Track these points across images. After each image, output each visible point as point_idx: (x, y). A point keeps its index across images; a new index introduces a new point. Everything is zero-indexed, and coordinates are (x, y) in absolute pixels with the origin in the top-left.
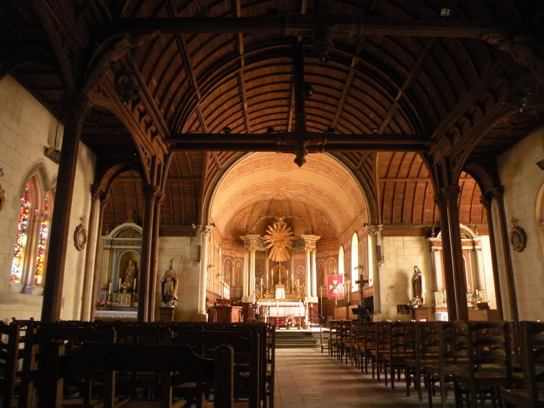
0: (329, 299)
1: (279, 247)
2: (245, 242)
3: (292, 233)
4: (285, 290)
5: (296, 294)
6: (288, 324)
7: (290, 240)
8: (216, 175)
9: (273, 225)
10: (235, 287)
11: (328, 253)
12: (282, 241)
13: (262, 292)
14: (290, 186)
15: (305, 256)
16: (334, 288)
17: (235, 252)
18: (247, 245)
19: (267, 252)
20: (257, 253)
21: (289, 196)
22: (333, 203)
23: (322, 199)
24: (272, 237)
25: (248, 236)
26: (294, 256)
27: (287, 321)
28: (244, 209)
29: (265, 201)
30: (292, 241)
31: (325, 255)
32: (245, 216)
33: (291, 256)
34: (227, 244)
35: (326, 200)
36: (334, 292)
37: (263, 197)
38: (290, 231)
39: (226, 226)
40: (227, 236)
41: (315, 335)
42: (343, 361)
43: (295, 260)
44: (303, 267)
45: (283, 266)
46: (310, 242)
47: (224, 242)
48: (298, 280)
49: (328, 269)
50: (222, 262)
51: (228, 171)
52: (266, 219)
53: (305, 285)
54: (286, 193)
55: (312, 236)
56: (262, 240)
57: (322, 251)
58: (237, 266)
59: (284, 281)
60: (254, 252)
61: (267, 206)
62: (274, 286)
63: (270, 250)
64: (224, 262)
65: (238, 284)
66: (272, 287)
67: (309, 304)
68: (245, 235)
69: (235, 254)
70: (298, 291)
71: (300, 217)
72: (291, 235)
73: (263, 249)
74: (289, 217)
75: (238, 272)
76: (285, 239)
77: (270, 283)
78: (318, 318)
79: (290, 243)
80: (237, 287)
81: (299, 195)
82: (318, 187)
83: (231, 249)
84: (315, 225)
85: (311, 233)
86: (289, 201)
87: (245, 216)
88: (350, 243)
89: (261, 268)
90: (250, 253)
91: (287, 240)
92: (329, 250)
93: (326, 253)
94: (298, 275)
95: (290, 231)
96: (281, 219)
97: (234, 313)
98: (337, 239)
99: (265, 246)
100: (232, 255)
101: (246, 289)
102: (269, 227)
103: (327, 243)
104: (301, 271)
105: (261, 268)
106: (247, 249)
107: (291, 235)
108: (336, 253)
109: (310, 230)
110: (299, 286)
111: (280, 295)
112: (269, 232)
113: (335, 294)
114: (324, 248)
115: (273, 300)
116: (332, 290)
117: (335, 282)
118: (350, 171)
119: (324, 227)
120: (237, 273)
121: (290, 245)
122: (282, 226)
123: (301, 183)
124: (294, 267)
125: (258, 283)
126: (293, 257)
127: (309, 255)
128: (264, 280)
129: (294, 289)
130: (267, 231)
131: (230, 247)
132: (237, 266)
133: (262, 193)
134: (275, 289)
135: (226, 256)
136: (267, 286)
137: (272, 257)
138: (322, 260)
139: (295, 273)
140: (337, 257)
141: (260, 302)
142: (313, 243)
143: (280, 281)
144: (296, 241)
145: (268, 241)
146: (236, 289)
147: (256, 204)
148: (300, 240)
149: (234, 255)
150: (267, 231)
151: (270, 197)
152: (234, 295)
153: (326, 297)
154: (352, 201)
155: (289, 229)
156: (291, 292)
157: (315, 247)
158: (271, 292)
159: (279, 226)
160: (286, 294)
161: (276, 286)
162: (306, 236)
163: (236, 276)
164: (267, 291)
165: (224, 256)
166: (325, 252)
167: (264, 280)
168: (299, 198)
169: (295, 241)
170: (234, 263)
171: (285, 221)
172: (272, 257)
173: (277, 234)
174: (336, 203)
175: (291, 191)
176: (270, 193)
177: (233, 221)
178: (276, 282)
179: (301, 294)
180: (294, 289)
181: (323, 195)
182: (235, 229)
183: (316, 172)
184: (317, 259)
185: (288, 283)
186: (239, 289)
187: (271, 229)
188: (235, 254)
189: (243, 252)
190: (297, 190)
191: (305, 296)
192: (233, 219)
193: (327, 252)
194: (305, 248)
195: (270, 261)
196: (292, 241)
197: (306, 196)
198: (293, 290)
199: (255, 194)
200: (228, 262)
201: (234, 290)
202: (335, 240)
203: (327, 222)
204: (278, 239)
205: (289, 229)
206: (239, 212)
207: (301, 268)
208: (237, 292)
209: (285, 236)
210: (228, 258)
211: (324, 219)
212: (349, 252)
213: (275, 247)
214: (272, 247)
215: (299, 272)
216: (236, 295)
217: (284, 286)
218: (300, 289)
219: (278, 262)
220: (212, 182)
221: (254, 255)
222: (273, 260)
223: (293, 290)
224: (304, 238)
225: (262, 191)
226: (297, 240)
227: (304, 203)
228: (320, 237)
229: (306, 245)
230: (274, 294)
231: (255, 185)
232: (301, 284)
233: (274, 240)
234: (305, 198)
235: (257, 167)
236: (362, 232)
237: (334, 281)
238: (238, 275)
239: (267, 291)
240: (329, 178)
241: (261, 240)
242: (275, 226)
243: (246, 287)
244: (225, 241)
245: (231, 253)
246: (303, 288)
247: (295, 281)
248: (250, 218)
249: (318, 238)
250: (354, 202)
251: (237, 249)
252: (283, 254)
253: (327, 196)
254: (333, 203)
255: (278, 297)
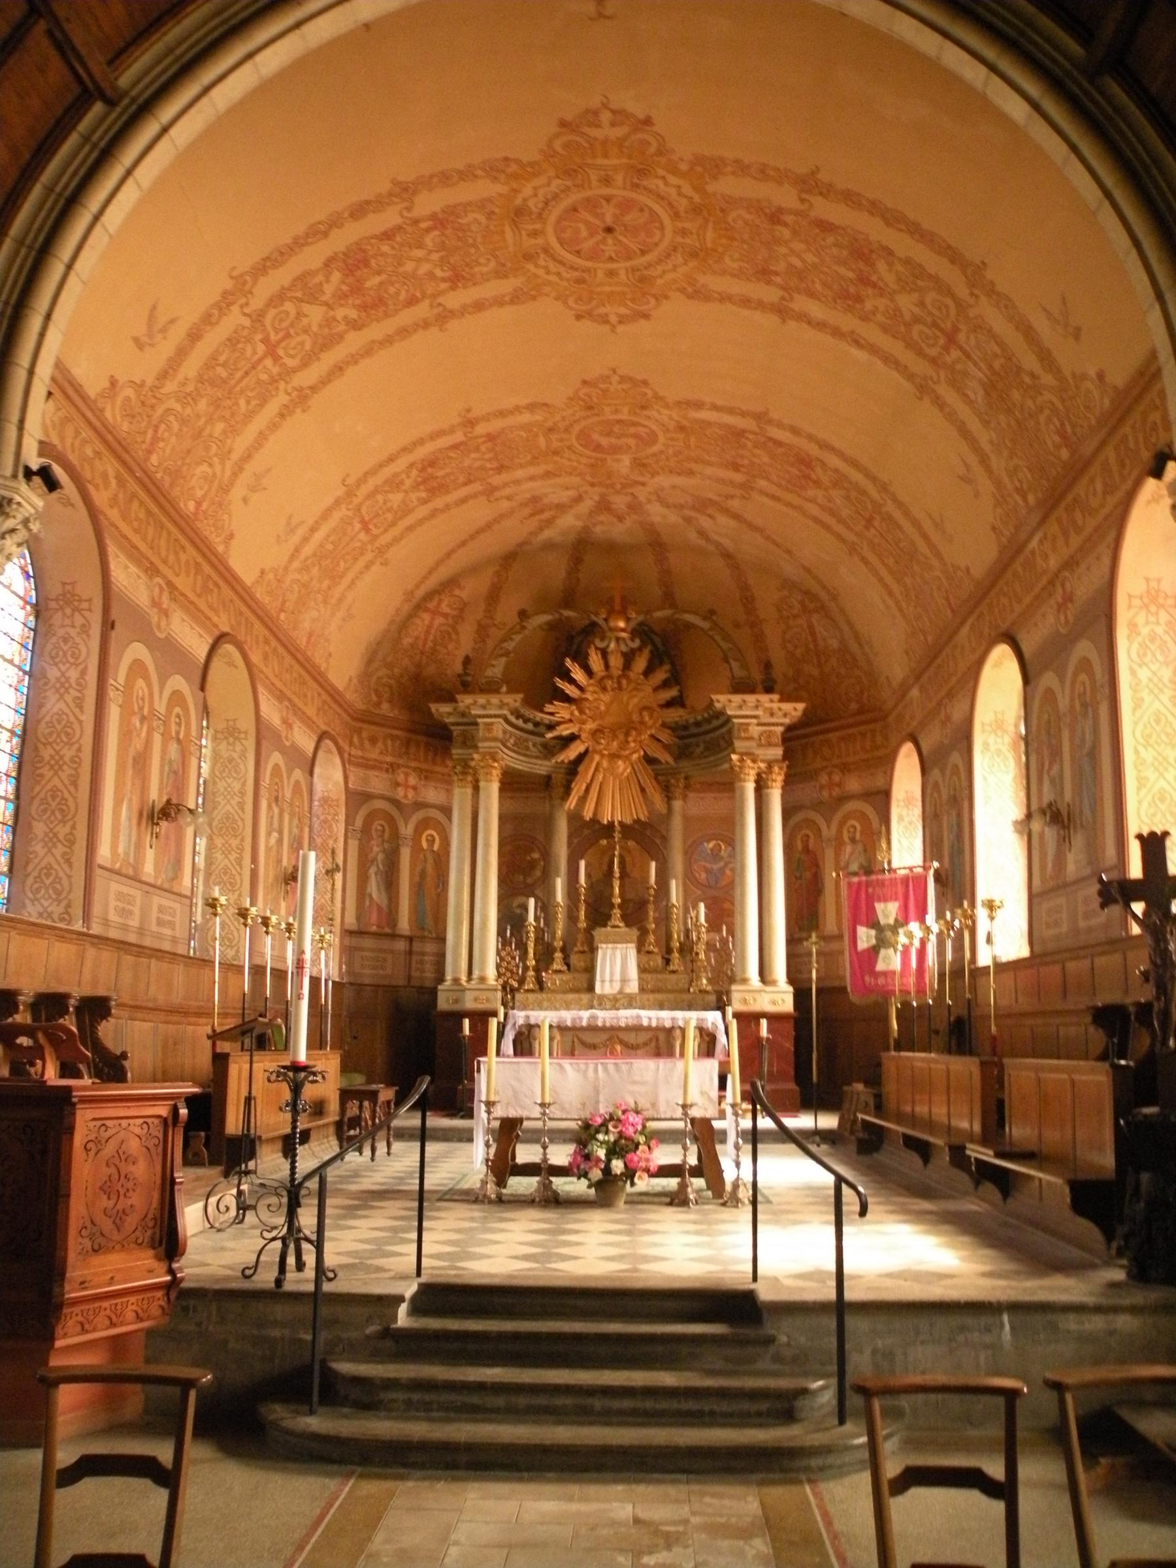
0: (854, 998)
1: (614, 757)
2: (456, 731)
3: (673, 693)
4: (639, 951)
5: (693, 972)
6: (607, 1171)
7: (664, 725)
8: (73, 140)
9: (587, 655)
10: (410, 939)
11: (839, 785)
12: (627, 727)
13: (531, 962)
14: (653, 438)
15: (732, 798)
16: (883, 942)
17: (412, 780)
18: (464, 744)
19: (558, 778)
20: (512, 783)
21: (657, 513)
22: (869, 522)
23: (813, 509)
24: (581, 712)
25: (465, 700)
26: (685, 798)
27: (601, 1153)
28: (451, 583)
29: (549, 546)
30: (674, 728)
31: (825, 794)
32: (460, 617)
33: (669, 799)
34: (373, 740)
35: (832, 513)
36: (880, 966)
37: (534, 523)
38: (665, 684)
39: (370, 661)
40: (378, 704)
41: (784, 1332)
42: (556, 444)
43: (687, 819)
44: (724, 851)
45: (631, 843)
46: (755, 730)
47: (359, 731)
48: (702, 906)
49: (837, 855)
50: (349, 821)
51: (167, 112)
52: (552, 627)
53: (731, 932)
54: (642, 494)
55: (764, 698)
56: (536, 724)
57: (810, 776)
58: (425, 845)
59: (634, 915)
60: (496, 774)
61: (563, 574)
62: (589, 931)
63: (573, 769)
64: (359, 822)
65: (429, 922)
66: (581, 937)
67: (756, 1017)
68: (452, 699)
69: (415, 788)
70: (702, 956)
71: (710, 614)
72: (669, 704)
73: (542, 767)
74: (659, 614)
75: (430, 869)
76: (642, 723)
77: (572, 918)
78: (792, 1086)
79: (665, 737)
80: (423, 939)
81: (703, 505)
82: (795, 431)
83: (393, 768)
84: (777, 655)
85: (760, 687)
86: (656, 544)
87: (460, 617)
88: (957, 714)
89: (536, 855)
90: (476, 789)
91: (652, 725)
92: (845, 768)
93: (831, 785)
94: (697, 883)
95: (665, 684)
96: (622, 624)
97: (95, 1145)
98: (885, 718)
99: (549, 750)
100: (400, 792)
101: (457, 945)
102: (568, 662)
103: (832, 736)
104: (715, 867)
105: (536, 855)
106: (465, 764)
107: (669, 704)
108: (880, 782)
109: (757, 676)
110: (704, 936)
111: (617, 977)
112: (571, 690)
113: (885, 974)
114: (818, 763)
115: (585, 997)
116: (874, 951)
117: (887, 911)
118: (1033, 88)
119: (820, 665)
120: (423, 874)
121: (666, 747)
122: (628, 659)
123: (705, 415)
124: (686, 853)
125: (511, 921)
126: (677, 804)
127: (750, 787)
128: (545, 907)
129: (681, 950)
130: (561, 684)
131: (389, 759)
132: (425, 845)
133: (528, 489)
134: (592, 950)
135: (367, 797)
136: (559, 933)
137: (583, 799)
138: (812, 815)
139: (689, 877)
140: (882, 798)
141: (524, 1007)
142: (770, 734)
143: (617, 912)
144: (694, 730)
145: (565, 731)
146: (417, 946)
147: (509, 559)
148: (708, 721)
149: (411, 794)
150: (561, 684)
151: (569, 522)
152: (409, 978)
153: (836, 984)
154: (984, 461)
155: (661, 675)
156: (667, 962)
157: (779, 752)
158: (574, 959)
159: (616, 662)
160: (642, 970)
161: (599, 933)
162: (737, 699)
163: (418, 888)
164: (558, 955)
165: (356, 798)
166: (824, 779)
167: (545, 907)
168: (705, 522)
169: (686, 728)
170: (407, 830)
171: (642, 632)
172: (583, 799)
173: (606, 697)
174: (888, 518)
175: (664, 481)
176: (565, 496)
177: (407, 641)
178: (599, 916)
179: (713, 970)
180: (681, 950)
181: (818, 483)
182: (417, 678)
183: (781, 311)
184: (787, 815)
185: (656, 921)
186: (430, 947)
187: (578, 674)
188: (415, 788)
189: (447, 782)
190: (691, 473)
191: (732, 980)
192: (403, 625)
193: (836, 778)
194: (734, 757)
195: (575, 818)
196: (674, 728)
197: (735, 504)
198: (676, 955)
199: (490, 492)
200: (377, 825)
201: (410, 952)
202: (875, 721)
203: (834, 644)
204: (610, 720)
205: (661, 675)
206: (429, 596)
207: (715, 855)
208: (421, 962)
209: (646, 708)
210: (379, 804)
211: (819, 629)
212: (956, 758)
213: (597, 758)
214: (581, 758)
215: (708, 871)
216: (414, 974)
217: (634, 933)
218: (710, 946)
219: (611, 825)
220: (47, 176)
221: (495, 787)
222: (588, 814)
223: (676, 955)
224: (729, 712)
225: (520, 474)
226: (698, 724)
227: (727, 556)
228: (801, 706)
229: (738, 744)
230: (590, 970)
231: (480, 430)
232: (714, 924)
233: (590, 726)
234: (732, 523)
235: (457, 279)
236: (1051, 619)
237: (879, 907)
238: (430, 880)
239: (558, 955)
240: (857, 343)
241: (530, 726)
242: (595, 661)
243: (458, 937)
244: (368, 730)
245: (397, 784)
246: (724, 942)
247: (686, 911)
248: (482, 631)
249: (796, 710)
250: (998, 464)
251: (424, 766)
252: (635, 789)
253: (840, 480)
254: (869, 522)
255: (605, 985)
